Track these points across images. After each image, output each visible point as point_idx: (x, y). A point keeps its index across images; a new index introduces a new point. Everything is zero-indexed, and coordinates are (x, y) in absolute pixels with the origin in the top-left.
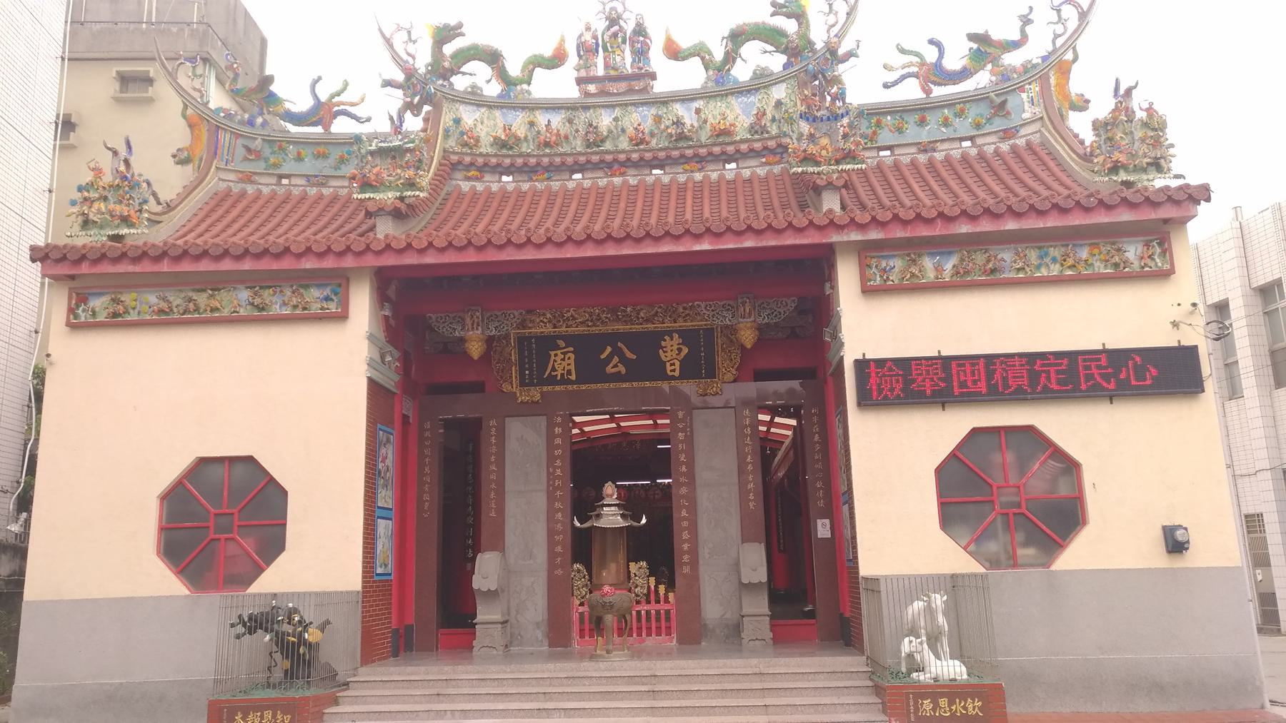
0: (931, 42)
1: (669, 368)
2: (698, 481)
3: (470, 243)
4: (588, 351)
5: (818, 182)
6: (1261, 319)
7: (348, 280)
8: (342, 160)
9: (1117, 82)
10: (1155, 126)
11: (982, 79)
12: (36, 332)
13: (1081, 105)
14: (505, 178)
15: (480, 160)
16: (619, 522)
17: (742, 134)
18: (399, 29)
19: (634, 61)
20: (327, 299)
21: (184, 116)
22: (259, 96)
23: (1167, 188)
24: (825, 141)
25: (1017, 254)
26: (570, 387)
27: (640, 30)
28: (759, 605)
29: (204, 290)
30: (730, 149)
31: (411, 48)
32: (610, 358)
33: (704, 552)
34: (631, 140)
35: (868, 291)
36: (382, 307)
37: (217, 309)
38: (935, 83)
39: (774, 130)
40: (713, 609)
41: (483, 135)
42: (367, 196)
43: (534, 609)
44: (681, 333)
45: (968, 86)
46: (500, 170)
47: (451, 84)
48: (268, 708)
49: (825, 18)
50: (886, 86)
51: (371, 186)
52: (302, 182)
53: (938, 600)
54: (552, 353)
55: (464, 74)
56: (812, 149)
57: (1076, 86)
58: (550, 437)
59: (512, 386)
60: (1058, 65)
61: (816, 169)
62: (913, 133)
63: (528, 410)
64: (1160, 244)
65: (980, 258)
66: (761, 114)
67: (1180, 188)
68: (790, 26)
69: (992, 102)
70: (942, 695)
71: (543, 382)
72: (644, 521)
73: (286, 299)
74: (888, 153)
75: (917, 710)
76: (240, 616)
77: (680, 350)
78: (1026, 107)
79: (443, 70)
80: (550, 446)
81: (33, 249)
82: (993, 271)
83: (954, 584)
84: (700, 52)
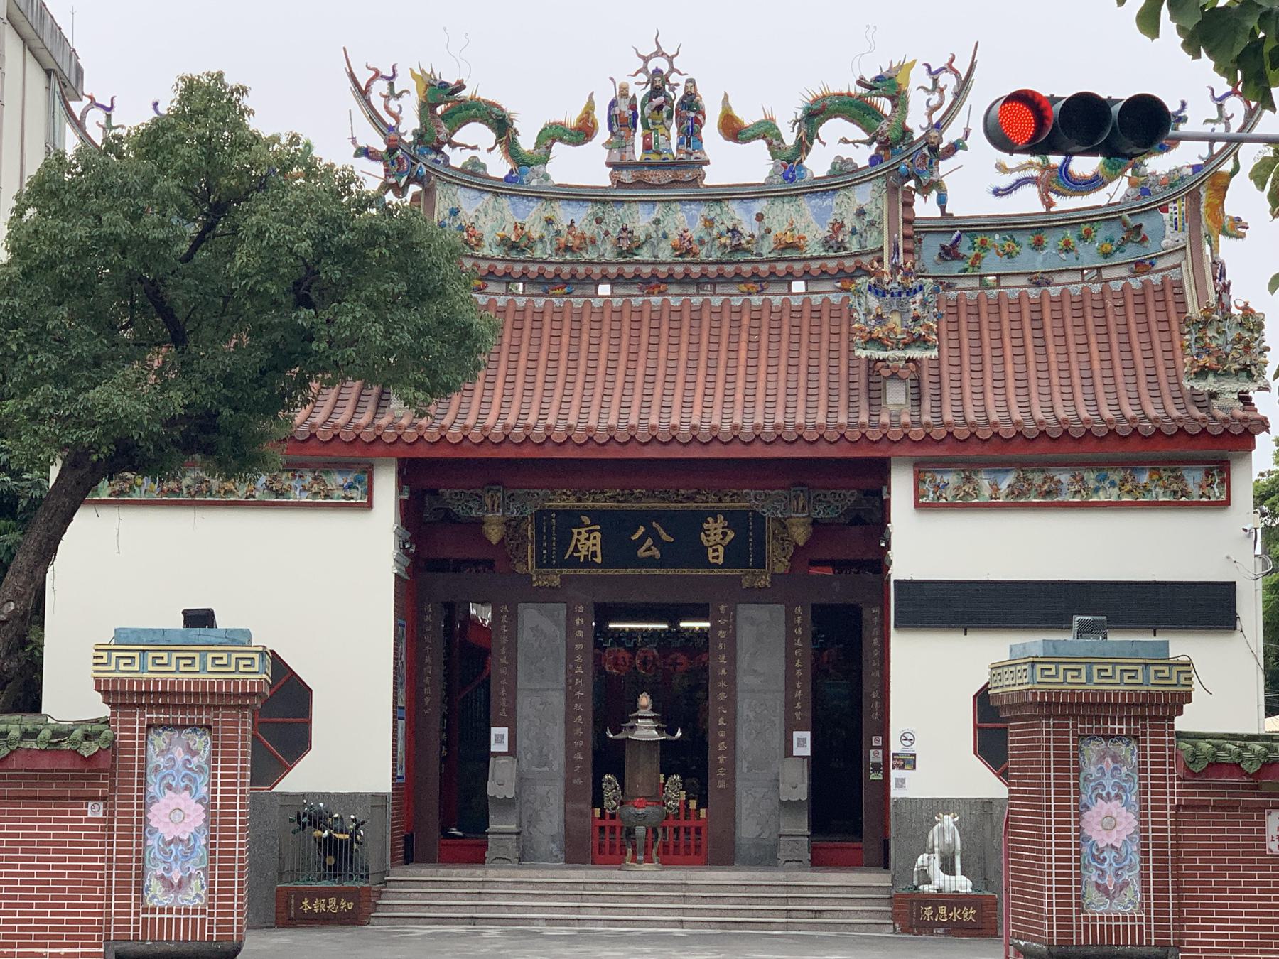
1: (711, 554)
7: (372, 466)
16: (654, 736)
19: (681, 142)
20: (350, 487)
25: (1074, 477)
27: (691, 102)
32: (642, 539)
33: (742, 766)
34: (675, 249)
37: (231, 491)
38: (1058, 193)
39: (855, 248)
40: (747, 829)
43: (551, 822)
45: (1098, 199)
46: (507, 278)
47: (447, 159)
49: (926, 96)
50: (997, 192)
54: (575, 531)
56: (878, 331)
58: (570, 629)
63: (544, 596)
64: (1221, 472)
65: (1037, 478)
66: (838, 226)
68: (885, 106)
69: (1125, 224)
70: (943, 903)
72: (679, 734)
73: (307, 484)
75: (919, 914)
77: (724, 534)
78: (1168, 232)
79: (429, 141)
82: (1048, 493)
84: (766, 131)
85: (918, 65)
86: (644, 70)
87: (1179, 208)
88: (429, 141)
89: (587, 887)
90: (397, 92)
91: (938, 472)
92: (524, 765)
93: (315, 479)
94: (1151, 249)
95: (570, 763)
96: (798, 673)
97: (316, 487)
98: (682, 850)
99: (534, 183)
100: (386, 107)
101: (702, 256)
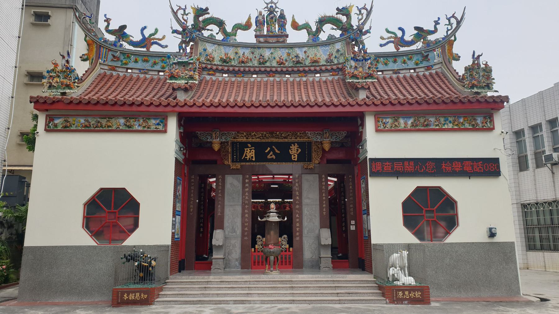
0: (400, 29)
1: (293, 157)
2: (303, 203)
3: (220, 104)
4: (260, 148)
5: (358, 86)
6: (515, 144)
7: (167, 116)
8: (155, 63)
9: (474, 52)
10: (488, 70)
11: (419, 45)
12: (8, 129)
13: (457, 58)
14: (224, 75)
15: (215, 67)
17: (322, 62)
18: (180, 8)
20: (158, 124)
21: (85, 40)
22: (119, 34)
23: (493, 97)
24: (361, 69)
25: (436, 119)
26: (252, 163)
27: (282, 16)
28: (327, 254)
29: (105, 118)
30: (318, 68)
31: (185, 17)
32: (269, 152)
33: (305, 231)
34: (278, 62)
35: (377, 130)
36: (180, 128)
37: (110, 126)
39: (336, 61)
40: (308, 254)
41: (216, 56)
42: (173, 81)
43: (236, 253)
44: (299, 143)
45: (413, 47)
46: (223, 72)
47: (202, 34)
48: (138, 292)
51: (174, 77)
52: (137, 71)
53: (405, 253)
54: (246, 149)
55: (208, 30)
56: (356, 72)
57: (456, 49)
58: (244, 183)
59: (229, 162)
60: (448, 42)
61: (357, 81)
62: (392, 66)
63: (234, 172)
65: (422, 120)
67: (498, 97)
68: (344, 19)
69: (423, 54)
70: (406, 290)
71: (241, 161)
72: (286, 219)
73: (141, 123)
74: (380, 73)
76: (125, 255)
77: (297, 150)
79: (198, 27)
80: (244, 187)
81: (31, 98)
82: (427, 125)
83: (408, 247)
84: (306, 27)
85: (355, 6)
86: (267, 7)
87: (438, 51)
88: (198, 27)
89: (251, 283)
90: (186, 13)
91: (384, 118)
92: (227, 233)
93: (144, 121)
94: (431, 63)
95: (243, 231)
96: (324, 198)
97: (144, 125)
98: (284, 263)
99: (232, 41)
100: (183, 18)
101: (287, 64)
